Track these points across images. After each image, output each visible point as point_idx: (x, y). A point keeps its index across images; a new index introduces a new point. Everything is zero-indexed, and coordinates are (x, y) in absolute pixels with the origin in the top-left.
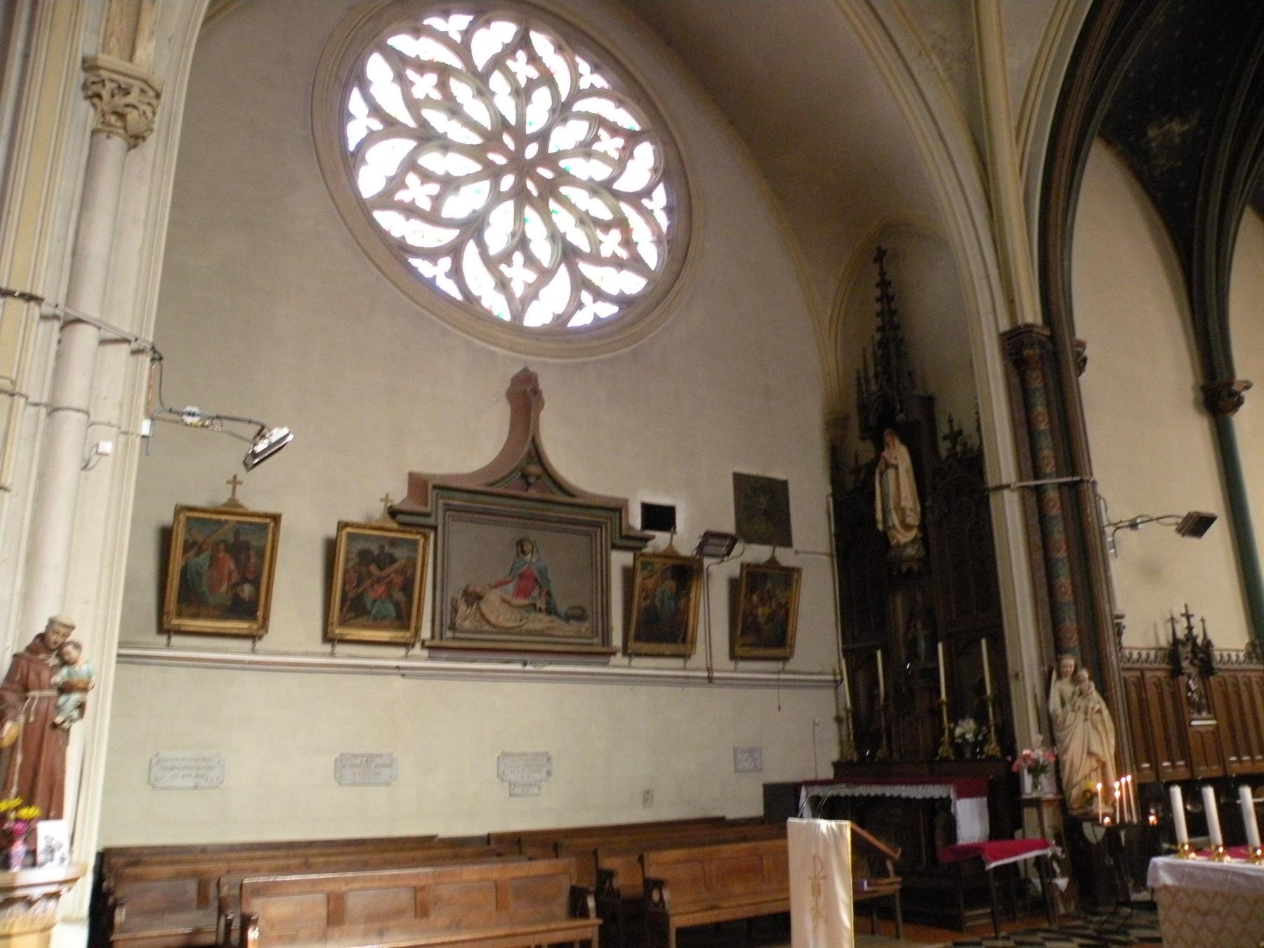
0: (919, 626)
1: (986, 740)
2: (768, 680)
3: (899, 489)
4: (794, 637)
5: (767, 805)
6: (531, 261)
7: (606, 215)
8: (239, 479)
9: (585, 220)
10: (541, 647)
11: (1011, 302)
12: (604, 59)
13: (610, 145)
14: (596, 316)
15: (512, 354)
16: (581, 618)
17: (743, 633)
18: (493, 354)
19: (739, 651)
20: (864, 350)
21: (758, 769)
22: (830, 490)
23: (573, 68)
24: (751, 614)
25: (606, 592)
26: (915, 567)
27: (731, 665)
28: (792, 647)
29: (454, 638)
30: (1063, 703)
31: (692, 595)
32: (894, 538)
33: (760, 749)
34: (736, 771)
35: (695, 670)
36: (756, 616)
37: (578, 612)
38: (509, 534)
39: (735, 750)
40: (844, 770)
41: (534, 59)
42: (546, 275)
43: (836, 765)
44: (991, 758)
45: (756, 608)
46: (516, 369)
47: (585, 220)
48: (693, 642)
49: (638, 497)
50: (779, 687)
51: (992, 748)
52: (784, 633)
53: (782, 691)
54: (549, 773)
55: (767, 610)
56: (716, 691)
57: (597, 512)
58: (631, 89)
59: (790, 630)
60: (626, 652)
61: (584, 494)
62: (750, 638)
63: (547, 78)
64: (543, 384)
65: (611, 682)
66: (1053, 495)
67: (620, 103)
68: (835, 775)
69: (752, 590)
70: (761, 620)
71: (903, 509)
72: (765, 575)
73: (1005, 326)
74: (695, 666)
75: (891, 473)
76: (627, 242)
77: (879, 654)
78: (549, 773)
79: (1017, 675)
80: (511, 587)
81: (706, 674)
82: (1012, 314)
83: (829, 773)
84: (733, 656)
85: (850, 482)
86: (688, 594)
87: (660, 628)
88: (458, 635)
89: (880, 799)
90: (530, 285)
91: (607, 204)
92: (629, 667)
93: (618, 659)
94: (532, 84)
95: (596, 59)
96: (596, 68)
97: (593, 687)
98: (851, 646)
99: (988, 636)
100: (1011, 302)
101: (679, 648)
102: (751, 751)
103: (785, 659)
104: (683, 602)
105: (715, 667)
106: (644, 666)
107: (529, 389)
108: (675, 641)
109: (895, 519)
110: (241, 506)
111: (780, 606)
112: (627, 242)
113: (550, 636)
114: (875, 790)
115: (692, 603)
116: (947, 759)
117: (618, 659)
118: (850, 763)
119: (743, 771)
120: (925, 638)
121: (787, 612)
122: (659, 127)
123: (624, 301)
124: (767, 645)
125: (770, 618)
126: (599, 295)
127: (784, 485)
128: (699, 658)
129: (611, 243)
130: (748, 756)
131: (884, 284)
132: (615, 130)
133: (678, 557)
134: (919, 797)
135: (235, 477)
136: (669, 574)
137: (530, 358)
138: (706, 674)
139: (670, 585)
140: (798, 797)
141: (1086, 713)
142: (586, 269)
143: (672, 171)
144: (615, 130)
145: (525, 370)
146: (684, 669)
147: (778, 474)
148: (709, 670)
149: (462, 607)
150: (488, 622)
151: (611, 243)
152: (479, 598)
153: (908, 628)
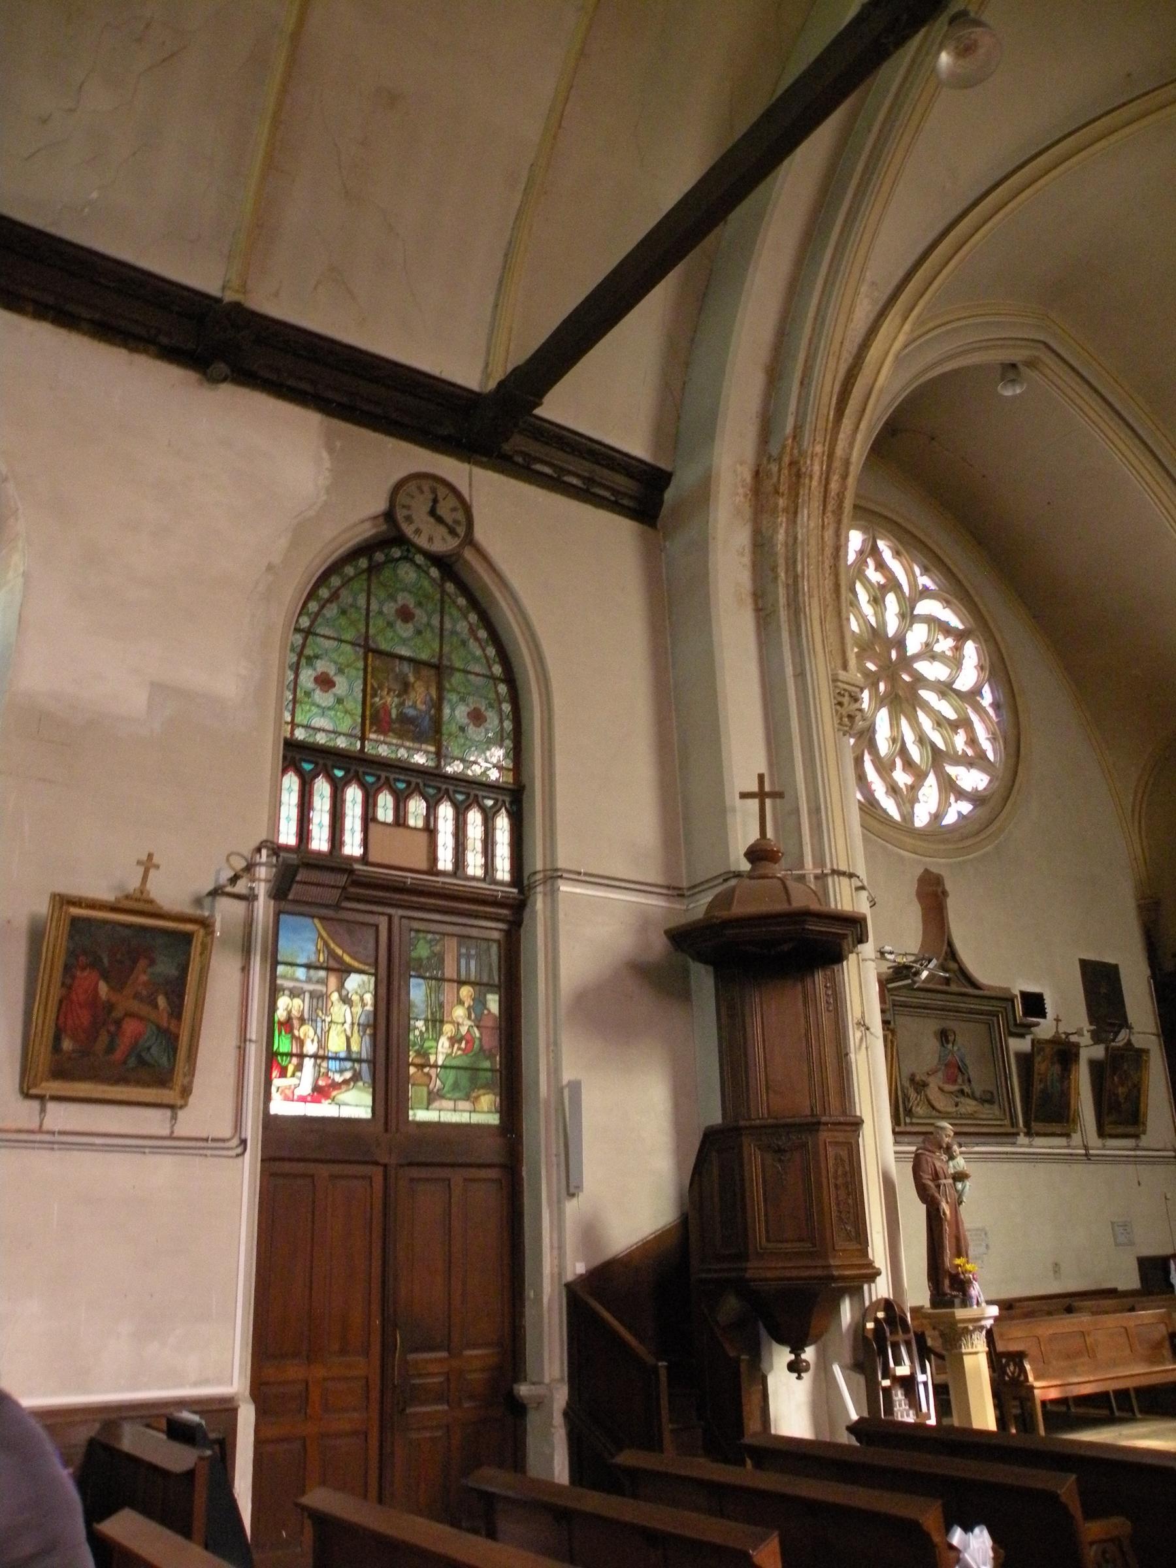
2: (1127, 1156)
4: (1145, 1114)
5: (1144, 1277)
6: (909, 764)
7: (951, 715)
8: (155, 860)
9: (940, 722)
10: (972, 1130)
12: (934, 562)
13: (945, 645)
14: (959, 813)
15: (913, 855)
16: (991, 1102)
18: (902, 859)
21: (1131, 1243)
22: (1148, 972)
23: (910, 574)
25: (1008, 1077)
28: (1144, 1124)
29: (912, 1124)
34: (1117, 1245)
36: (1117, 1095)
37: (988, 1097)
38: (932, 1026)
39: (1112, 1223)
41: (881, 566)
42: (920, 776)
46: (919, 871)
47: (940, 722)
49: (1021, 985)
50: (1135, 1163)
52: (1138, 1110)
54: (987, 1247)
57: (994, 1002)
58: (957, 591)
60: (1028, 1134)
61: (990, 988)
63: (892, 584)
64: (949, 886)
65: (1018, 1160)
67: (947, 603)
72: (1122, 1056)
76: (972, 741)
78: (987, 1247)
80: (940, 1074)
81: (1083, 1152)
84: (1101, 1134)
86: (1069, 1076)
87: (1047, 1112)
88: (914, 1121)
90: (964, 817)
91: (952, 705)
92: (1030, 1146)
93: (1022, 1139)
94: (883, 589)
95: (926, 562)
96: (926, 570)
97: (1006, 1166)
101: (1131, 1130)
102: (1124, 1225)
103: (1136, 1136)
105: (1090, 1144)
106: (1042, 1145)
107: (940, 890)
110: (151, 902)
111: (1135, 1086)
112: (972, 741)
113: (976, 1119)
115: (1073, 1085)
117: (1022, 1139)
121: (1139, 1091)
122: (980, 626)
123: (976, 798)
126: (961, 794)
127: (1116, 967)
128: (1076, 1138)
129: (960, 740)
130: (1122, 1230)
132: (947, 630)
135: (150, 856)
137: (928, 859)
138: (1083, 1152)
139: (1057, 1068)
142: (952, 770)
143: (998, 668)
144: (947, 630)
145: (926, 870)
147: (1110, 959)
148: (1086, 1148)
149: (913, 1094)
150: (933, 1108)
151: (960, 740)
152: (925, 1085)
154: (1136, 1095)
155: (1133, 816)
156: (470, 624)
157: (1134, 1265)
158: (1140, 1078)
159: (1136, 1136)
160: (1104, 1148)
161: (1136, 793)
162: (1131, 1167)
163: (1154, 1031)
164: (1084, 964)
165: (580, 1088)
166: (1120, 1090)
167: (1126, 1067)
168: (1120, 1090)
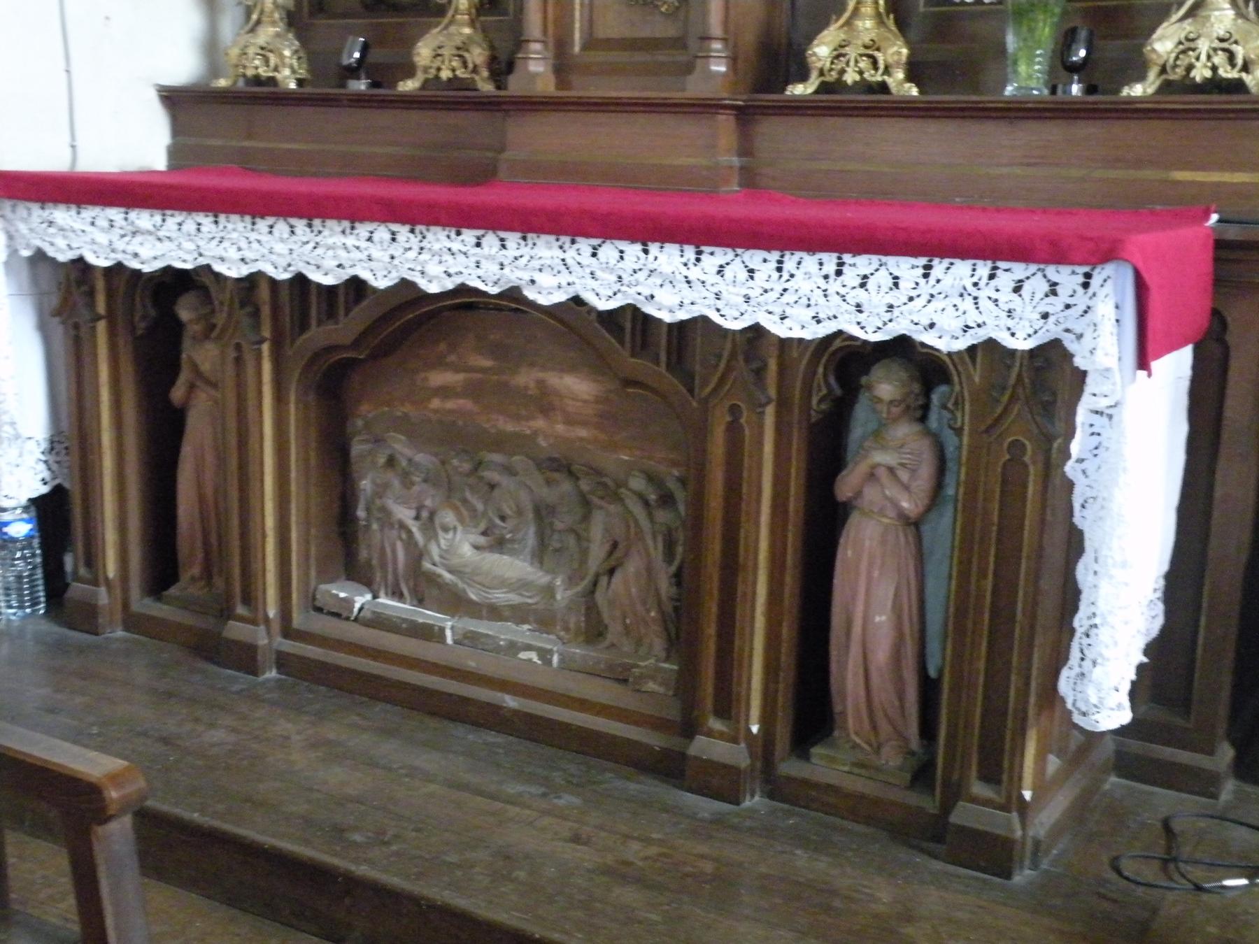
114: (440, 260)
116: (872, 102)
118: (260, 94)
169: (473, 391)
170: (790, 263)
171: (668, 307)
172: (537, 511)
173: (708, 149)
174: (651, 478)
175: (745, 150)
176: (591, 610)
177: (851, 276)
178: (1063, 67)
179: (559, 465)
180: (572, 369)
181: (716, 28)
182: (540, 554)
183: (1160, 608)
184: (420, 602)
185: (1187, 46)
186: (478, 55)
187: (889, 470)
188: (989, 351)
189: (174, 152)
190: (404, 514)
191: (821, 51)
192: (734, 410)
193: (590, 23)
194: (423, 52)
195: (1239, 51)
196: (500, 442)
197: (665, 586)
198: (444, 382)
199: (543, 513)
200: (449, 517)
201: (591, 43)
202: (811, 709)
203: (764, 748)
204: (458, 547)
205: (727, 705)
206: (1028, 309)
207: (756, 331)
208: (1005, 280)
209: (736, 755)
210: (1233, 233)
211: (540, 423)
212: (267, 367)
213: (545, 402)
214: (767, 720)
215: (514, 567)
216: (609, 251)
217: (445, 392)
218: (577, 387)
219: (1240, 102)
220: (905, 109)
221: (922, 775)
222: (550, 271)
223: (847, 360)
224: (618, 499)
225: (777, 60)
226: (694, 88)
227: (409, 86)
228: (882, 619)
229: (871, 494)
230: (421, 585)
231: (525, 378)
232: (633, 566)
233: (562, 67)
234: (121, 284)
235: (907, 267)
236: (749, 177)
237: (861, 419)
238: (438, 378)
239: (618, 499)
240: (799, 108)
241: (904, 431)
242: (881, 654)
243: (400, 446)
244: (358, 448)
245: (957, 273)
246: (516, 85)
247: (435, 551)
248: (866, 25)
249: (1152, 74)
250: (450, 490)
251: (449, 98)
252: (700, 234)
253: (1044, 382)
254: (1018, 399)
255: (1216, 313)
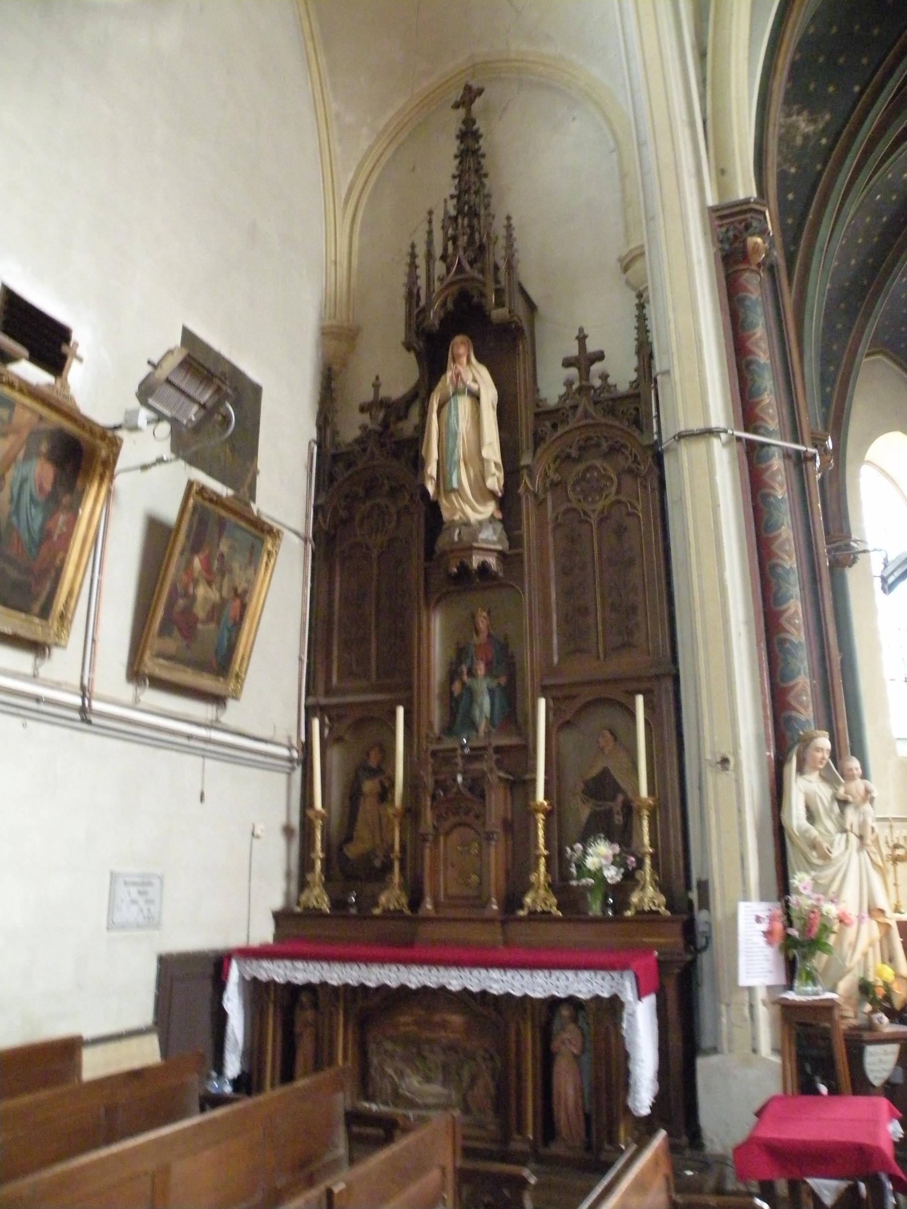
0: (481, 669)
1: (630, 878)
2: (189, 737)
3: (467, 432)
11: (722, 172)
17: (164, 630)
19: (152, 665)
20: (430, 213)
21: (152, 922)
22: (313, 434)
24: (186, 595)
26: (492, 561)
27: (127, 691)
30: (811, 816)
31: (85, 512)
32: (454, 510)
33: (161, 879)
34: (111, 926)
35: (57, 686)
36: (192, 599)
39: (114, 876)
40: (296, 931)
43: (280, 917)
44: (648, 917)
45: (196, 583)
48: (64, 619)
50: (204, 754)
51: (648, 897)
52: (232, 648)
53: (209, 763)
55: (214, 595)
56: (89, 741)
59: (241, 650)
62: (172, 645)
66: (777, 463)
68: (278, 936)
69: (196, 544)
70: (200, 611)
71: (482, 460)
73: (711, 200)
74: (57, 676)
75: (464, 404)
77: (400, 711)
79: (725, 761)
81: (78, 701)
82: (722, 187)
83: (264, 932)
84: (136, 673)
85: (352, 424)
89: (402, 996)
98: (323, 701)
99: (647, 694)
100: (722, 172)
101: (207, 682)
102: (144, 883)
104: (62, 518)
108: (23, 608)
109: (462, 477)
114: (416, 977)
116: (546, 916)
118: (312, 914)
119: (123, 927)
120: (491, 692)
121: (244, 607)
124: (201, 666)
125: (216, 611)
128: (63, 664)
131: (469, 135)
133: (72, 415)
134: (538, 994)
136: (44, 447)
138: (78, 701)
139: (41, 472)
140: (220, 985)
141: (861, 837)
146: (34, 677)
153: (453, 674)
154: (233, 614)
155: (346, 202)
156: (453, 1117)
157: (151, 971)
158: (251, 583)
159: (218, 700)
160: (134, 705)
161: (361, 166)
162: (192, 762)
163: (300, 528)
164: (188, 337)
165: (765, 1181)
166: (202, 591)
167: (224, 547)
168: (202, 591)
169: (417, 1023)
170: (535, 974)
171: (496, 989)
172: (444, 1068)
173: (491, 935)
174: (487, 1051)
175: (504, 932)
176: (464, 1100)
177: (554, 977)
178: (605, 905)
179: (452, 1048)
180: (454, 1013)
181: (493, 892)
182: (445, 1084)
183: (657, 1084)
184: (396, 1105)
185: (641, 900)
186: (404, 900)
187: (568, 1039)
188: (597, 998)
189: (277, 937)
190: (390, 1071)
191: (528, 900)
192: (518, 1023)
193: (446, 889)
194: (383, 899)
195: (656, 901)
196: (429, 1041)
197: (492, 1090)
198: (405, 1020)
199: (445, 1067)
200: (408, 1071)
201: (446, 896)
202: (548, 1128)
203: (534, 1145)
204: (413, 1083)
205: (521, 1129)
206: (606, 985)
207: (526, 997)
208: (599, 977)
209: (526, 1148)
210: (662, 958)
211: (443, 1034)
212: (341, 1018)
213: (444, 1025)
214: (534, 1135)
215: (436, 1088)
216: (475, 972)
217: (406, 1024)
218: (456, 1019)
219: (527, 508)
220: (557, 920)
221: (588, 1148)
222: (455, 980)
223: (553, 1003)
224: (474, 1059)
225: (512, 902)
226: (487, 914)
227: (377, 911)
228: (571, 1092)
229: (563, 1048)
230: (397, 1098)
231: (437, 1018)
232: (480, 1083)
233: (436, 904)
234: (346, 991)
235: (570, 974)
236: (506, 943)
237: (556, 1025)
238: (403, 1019)
239: (474, 1059)
240: (521, 920)
241: (571, 1027)
242: (571, 1102)
243: (388, 1046)
244: (372, 1047)
245: (586, 975)
246: (421, 913)
247: (404, 1086)
248: (542, 892)
249: (633, 909)
250: (408, 1060)
251: (390, 915)
252: (504, 965)
253: (612, 1008)
254: (850, 945)
255: (661, 983)
